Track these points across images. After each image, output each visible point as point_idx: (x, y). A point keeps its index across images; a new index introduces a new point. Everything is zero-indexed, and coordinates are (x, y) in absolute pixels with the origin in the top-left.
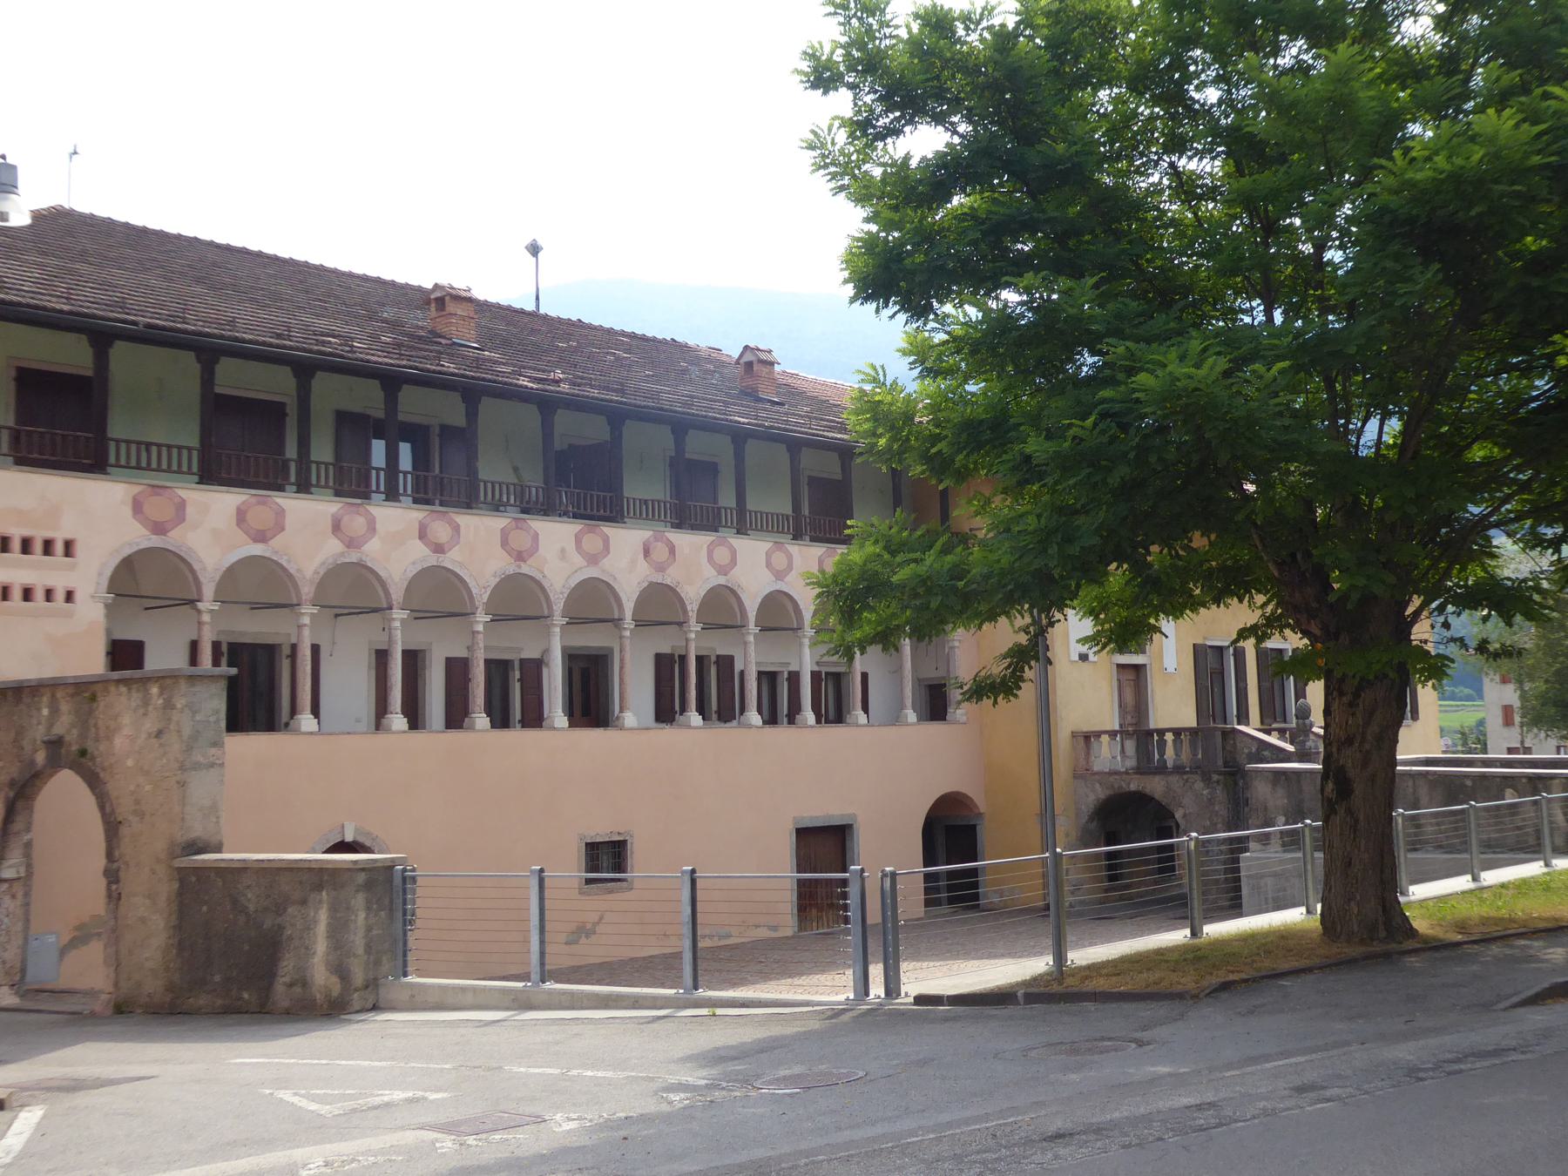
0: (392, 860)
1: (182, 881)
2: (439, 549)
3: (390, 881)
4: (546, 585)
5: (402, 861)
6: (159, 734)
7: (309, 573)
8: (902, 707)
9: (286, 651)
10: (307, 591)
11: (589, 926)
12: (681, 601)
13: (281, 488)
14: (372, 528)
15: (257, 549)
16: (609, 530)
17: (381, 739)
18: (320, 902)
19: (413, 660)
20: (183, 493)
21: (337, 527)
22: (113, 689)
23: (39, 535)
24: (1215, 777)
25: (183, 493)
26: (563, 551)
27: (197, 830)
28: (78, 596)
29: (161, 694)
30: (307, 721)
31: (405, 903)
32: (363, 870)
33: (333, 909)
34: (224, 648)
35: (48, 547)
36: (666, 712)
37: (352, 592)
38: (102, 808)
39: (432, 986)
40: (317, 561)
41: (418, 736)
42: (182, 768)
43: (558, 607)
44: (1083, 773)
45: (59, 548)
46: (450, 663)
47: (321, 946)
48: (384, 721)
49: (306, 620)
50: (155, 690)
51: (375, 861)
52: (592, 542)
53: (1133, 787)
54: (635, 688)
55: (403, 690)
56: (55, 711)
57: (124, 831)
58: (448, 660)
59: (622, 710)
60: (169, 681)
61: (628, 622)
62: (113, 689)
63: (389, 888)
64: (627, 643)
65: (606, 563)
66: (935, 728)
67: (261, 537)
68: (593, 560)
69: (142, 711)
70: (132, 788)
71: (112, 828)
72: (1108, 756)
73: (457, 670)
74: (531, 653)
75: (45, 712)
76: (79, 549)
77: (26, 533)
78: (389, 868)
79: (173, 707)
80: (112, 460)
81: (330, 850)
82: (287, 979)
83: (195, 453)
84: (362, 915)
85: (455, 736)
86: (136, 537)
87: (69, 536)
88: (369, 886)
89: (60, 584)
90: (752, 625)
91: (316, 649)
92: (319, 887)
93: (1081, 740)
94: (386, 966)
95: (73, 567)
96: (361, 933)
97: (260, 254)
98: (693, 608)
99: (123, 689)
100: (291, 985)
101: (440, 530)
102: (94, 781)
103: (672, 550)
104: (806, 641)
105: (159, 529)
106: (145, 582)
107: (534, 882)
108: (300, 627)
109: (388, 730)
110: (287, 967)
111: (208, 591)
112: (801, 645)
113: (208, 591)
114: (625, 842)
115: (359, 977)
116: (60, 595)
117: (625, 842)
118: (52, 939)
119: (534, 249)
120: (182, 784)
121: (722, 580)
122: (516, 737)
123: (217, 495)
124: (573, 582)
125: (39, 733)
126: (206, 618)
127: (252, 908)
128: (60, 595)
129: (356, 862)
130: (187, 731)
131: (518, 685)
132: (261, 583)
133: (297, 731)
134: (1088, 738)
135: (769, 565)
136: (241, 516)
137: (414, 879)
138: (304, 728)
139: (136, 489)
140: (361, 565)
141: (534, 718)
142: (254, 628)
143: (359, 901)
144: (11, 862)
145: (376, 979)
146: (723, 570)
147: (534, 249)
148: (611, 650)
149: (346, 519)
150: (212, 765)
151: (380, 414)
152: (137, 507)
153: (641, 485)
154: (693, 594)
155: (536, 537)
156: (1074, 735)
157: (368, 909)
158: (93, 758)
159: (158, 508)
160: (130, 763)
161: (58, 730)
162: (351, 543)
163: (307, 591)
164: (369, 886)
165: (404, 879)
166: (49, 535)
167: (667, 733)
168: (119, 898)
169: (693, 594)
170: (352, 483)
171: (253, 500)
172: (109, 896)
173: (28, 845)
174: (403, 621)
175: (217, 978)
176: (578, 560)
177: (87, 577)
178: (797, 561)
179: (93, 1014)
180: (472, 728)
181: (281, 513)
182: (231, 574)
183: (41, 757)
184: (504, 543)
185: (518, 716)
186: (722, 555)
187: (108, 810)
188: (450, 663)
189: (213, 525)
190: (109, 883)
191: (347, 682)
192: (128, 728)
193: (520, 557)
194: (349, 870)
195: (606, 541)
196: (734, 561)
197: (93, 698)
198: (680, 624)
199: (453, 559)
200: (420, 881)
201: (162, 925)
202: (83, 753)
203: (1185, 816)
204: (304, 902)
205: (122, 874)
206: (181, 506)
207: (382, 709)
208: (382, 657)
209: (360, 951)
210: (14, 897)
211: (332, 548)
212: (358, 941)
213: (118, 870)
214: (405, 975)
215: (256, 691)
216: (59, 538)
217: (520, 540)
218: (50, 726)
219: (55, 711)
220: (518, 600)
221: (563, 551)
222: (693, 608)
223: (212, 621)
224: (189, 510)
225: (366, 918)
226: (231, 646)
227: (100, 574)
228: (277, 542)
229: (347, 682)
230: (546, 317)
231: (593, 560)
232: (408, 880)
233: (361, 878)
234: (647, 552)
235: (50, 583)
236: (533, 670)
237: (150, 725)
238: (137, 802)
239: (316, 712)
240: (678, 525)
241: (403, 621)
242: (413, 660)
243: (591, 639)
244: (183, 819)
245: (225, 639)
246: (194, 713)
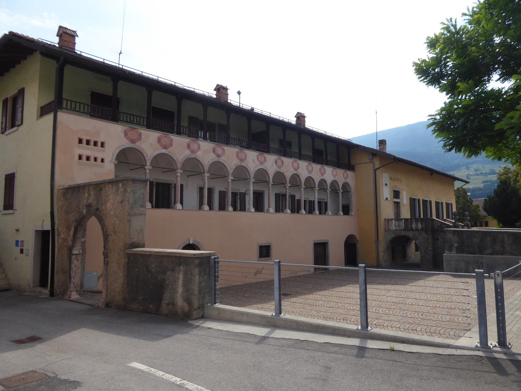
0: (210, 254)
1: (128, 258)
2: (218, 156)
3: (209, 262)
4: (249, 169)
5: (214, 254)
6: (122, 202)
7: (180, 161)
8: (338, 210)
9: (173, 186)
10: (179, 165)
11: (260, 270)
12: (285, 177)
13: (172, 133)
14: (199, 148)
15: (164, 151)
16: (266, 155)
17: (201, 212)
18: (180, 271)
19: (210, 190)
20: (141, 131)
21: (188, 146)
22: (107, 186)
24: (429, 232)
25: (141, 131)
26: (253, 160)
27: (135, 239)
28: (105, 161)
29: (123, 186)
30: (179, 206)
31: (215, 273)
32: (198, 258)
33: (185, 274)
34: (155, 184)
35: (95, 144)
36: (278, 210)
37: (193, 167)
38: (103, 230)
39: (228, 311)
40: (182, 157)
42: (129, 215)
43: (252, 176)
44: (387, 230)
45: (99, 144)
46: (220, 192)
47: (180, 289)
48: (202, 207)
49: (179, 174)
50: (120, 185)
51: (203, 254)
52: (261, 158)
53: (403, 234)
54: (269, 201)
55: (207, 199)
56: (89, 195)
57: (110, 238)
58: (220, 191)
59: (269, 207)
60: (125, 182)
61: (271, 182)
62: (107, 186)
63: (208, 265)
64: (271, 188)
65: (265, 164)
66: (346, 217)
67: (165, 147)
68: (262, 163)
69: (116, 193)
70: (113, 222)
71: (106, 237)
72: (393, 226)
73: (223, 195)
74: (243, 191)
75: (86, 195)
76: (106, 145)
77: (88, 138)
78: (208, 257)
79: (126, 191)
81: (185, 248)
82: (166, 302)
83: (145, 119)
84: (197, 277)
85: (222, 213)
86: (125, 143)
87: (103, 141)
88: (200, 265)
89: (99, 156)
90: (303, 185)
91: (182, 186)
92: (180, 264)
93: (387, 222)
94: (207, 299)
95: (104, 151)
96: (197, 285)
98: (288, 179)
99: (110, 186)
100: (168, 304)
101: (219, 150)
102: (101, 220)
103: (283, 163)
104: (316, 191)
105: (133, 141)
106: (127, 158)
107: (276, 267)
108: (177, 176)
109: (203, 210)
110: (167, 296)
111: (148, 163)
112: (315, 192)
113: (148, 163)
114: (270, 246)
115: (196, 304)
116: (99, 160)
117: (270, 246)
118: (96, 273)
119: (239, 93)
120: (129, 221)
121: (295, 172)
122: (239, 214)
123: (152, 133)
124: (256, 169)
125: (85, 202)
126: (148, 171)
127: (153, 270)
128: (99, 160)
129: (195, 255)
130: (131, 201)
131: (239, 200)
132: (163, 162)
133: (176, 209)
134: (388, 221)
135: (307, 169)
136: (159, 140)
137: (218, 262)
138: (178, 208)
139: (126, 128)
140: (196, 159)
141: (243, 208)
142: (164, 178)
143: (196, 271)
144: (77, 248)
145: (203, 305)
146: (296, 169)
147: (239, 93)
148: (264, 191)
149: (191, 144)
150: (141, 214)
151: (202, 119)
152: (126, 134)
153: (274, 145)
154: (288, 175)
155: (246, 155)
156: (385, 220)
157: (200, 274)
158: (100, 212)
159: (133, 135)
160: (112, 213)
161: (90, 201)
162: (193, 152)
163: (179, 165)
164: (200, 265)
165: (215, 262)
166: (96, 139)
167: (280, 215)
168: (108, 264)
169: (288, 175)
170: (193, 134)
171: (163, 135)
172: (105, 263)
173: (84, 242)
174: (208, 177)
175: (141, 298)
176: (258, 163)
177: (109, 154)
178: (314, 169)
179: (98, 307)
180: (227, 210)
181: (172, 140)
182: (157, 158)
183: (84, 211)
184: (237, 156)
185: (239, 209)
186: (295, 165)
187: (105, 230)
188: (220, 192)
189: (150, 142)
190: (105, 258)
191: (191, 196)
192: (112, 201)
193: (242, 161)
194: (192, 258)
195: (265, 158)
196: (298, 167)
197: (101, 189)
198: (284, 184)
199: (223, 159)
200: (220, 264)
201: (122, 275)
202: (97, 209)
203: (419, 243)
204: (173, 270)
205: (109, 254)
206: (140, 135)
207: (201, 204)
208: (201, 190)
209: (197, 293)
210: (77, 260)
211: (187, 153)
212: (196, 289)
213: (108, 253)
214: (215, 303)
215: (163, 196)
217: (242, 155)
218: (88, 200)
219: (89, 195)
220: (241, 174)
221: (253, 160)
222: (288, 179)
223: (149, 174)
224: (143, 136)
225: (199, 279)
226: (157, 183)
227: (113, 154)
228: (171, 149)
229: (191, 196)
231: (262, 163)
232: (216, 262)
233: (197, 261)
234: (276, 163)
235: (96, 156)
236: (243, 196)
237: (119, 199)
238: (114, 228)
239: (182, 203)
240: (284, 156)
241: (208, 177)
242: (210, 190)
244: (129, 235)
245: (155, 181)
246: (134, 194)
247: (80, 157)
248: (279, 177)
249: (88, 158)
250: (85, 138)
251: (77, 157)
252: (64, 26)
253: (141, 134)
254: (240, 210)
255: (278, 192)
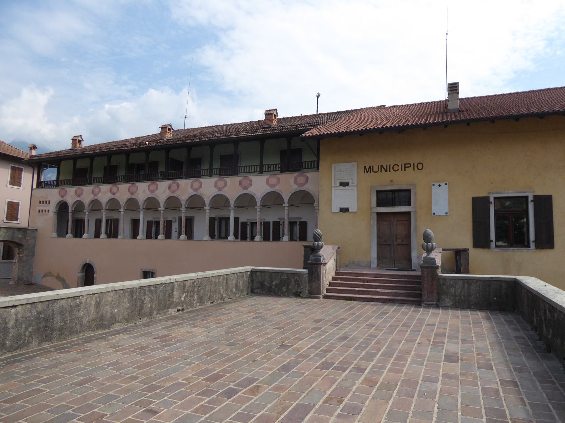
2: (114, 194)
16: (179, 181)
23: (45, 200)
41: (168, 241)
61: (162, 208)
65: (156, 192)
67: (79, 196)
80: (304, 167)
89: (47, 208)
97: (191, 129)
111: (141, 206)
139: (267, 177)
147: (318, 97)
162: (95, 195)
176: (148, 192)
193: (132, 194)
199: (117, 196)
216: (48, 200)
217: (133, 189)
221: (144, 190)
230: (188, 129)
243: (114, 215)
247: (39, 211)
248: (132, 204)
249: (42, 211)
250: (41, 200)
251: (38, 211)
252: (460, 85)
253: (279, 178)
254: (274, 239)
255: (151, 219)
